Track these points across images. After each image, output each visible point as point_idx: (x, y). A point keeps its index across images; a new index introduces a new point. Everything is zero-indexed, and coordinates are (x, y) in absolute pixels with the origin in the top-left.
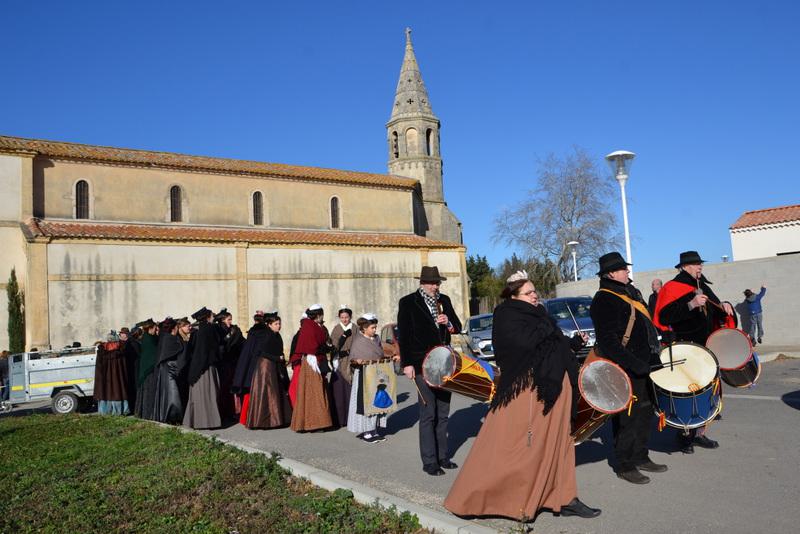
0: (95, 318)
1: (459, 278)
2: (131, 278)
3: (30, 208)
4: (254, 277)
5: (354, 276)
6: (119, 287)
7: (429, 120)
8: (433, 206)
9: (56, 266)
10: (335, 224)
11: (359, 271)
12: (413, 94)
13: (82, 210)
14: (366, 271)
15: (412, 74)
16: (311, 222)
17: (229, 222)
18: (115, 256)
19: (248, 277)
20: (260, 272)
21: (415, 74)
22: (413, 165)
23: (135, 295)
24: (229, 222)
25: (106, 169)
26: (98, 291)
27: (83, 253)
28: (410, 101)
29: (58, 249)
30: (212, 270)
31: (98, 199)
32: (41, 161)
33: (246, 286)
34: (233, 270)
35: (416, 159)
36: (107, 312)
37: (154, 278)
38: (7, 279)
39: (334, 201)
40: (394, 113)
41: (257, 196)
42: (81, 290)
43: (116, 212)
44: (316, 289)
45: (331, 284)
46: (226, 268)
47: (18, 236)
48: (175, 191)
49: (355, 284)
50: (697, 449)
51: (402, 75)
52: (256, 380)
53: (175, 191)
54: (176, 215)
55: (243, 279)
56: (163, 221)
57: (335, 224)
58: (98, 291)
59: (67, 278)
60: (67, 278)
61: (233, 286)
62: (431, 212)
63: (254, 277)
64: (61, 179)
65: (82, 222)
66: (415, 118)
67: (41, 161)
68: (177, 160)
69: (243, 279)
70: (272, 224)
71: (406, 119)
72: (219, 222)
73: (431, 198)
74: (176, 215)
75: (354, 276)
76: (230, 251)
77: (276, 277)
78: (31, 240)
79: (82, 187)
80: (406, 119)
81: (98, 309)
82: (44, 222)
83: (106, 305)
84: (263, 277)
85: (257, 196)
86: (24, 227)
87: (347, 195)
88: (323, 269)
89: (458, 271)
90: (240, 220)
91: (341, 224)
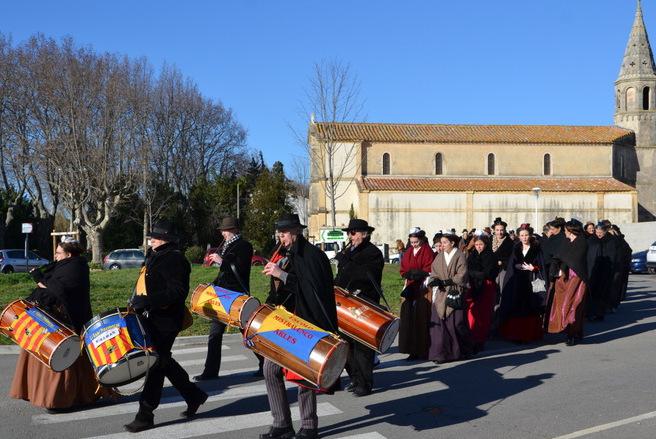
0: (390, 231)
1: (630, 213)
2: (408, 210)
3: (360, 170)
4: (477, 211)
5: (544, 211)
6: (402, 214)
7: (647, 79)
8: (645, 151)
9: (372, 205)
10: (547, 171)
11: (548, 207)
12: (636, 57)
13: (386, 170)
14: (553, 207)
15: (637, 39)
16: (529, 171)
17: (472, 174)
18: (400, 198)
19: (473, 211)
20: (480, 208)
21: (640, 39)
22: (630, 117)
23: (410, 220)
24: (472, 174)
25: (399, 146)
26: (392, 217)
27: (385, 197)
28: (633, 64)
29: (373, 195)
30: (453, 207)
31: (394, 163)
32: (366, 144)
33: (472, 216)
34: (464, 207)
35: (633, 113)
36: (395, 228)
37: (421, 211)
38: (349, 208)
39: (547, 157)
40: (621, 73)
41: (491, 157)
42: (383, 216)
43: (404, 171)
44: (516, 218)
45: (527, 216)
46: (460, 206)
47: (354, 187)
48: (439, 157)
49: (544, 216)
50: (549, 355)
51: (630, 40)
52: (590, 269)
53: (439, 157)
54: (439, 171)
55: (471, 212)
56: (431, 174)
57: (547, 171)
58: (392, 217)
59: (377, 210)
60: (377, 210)
61: (464, 216)
62: (642, 156)
63: (477, 211)
64: (376, 151)
65: (386, 177)
66: (634, 79)
67: (366, 144)
68: (553, 136)
69: (471, 212)
70: (500, 174)
71: (627, 81)
72: (466, 174)
73: (643, 145)
74: (439, 171)
75: (544, 211)
76: (462, 196)
77: (490, 211)
78: (361, 191)
79: (386, 157)
80: (627, 81)
81: (391, 226)
82: (368, 177)
83: (396, 224)
84: (483, 211)
85: (491, 157)
86: (358, 183)
87: (555, 151)
88: (522, 205)
89: (630, 207)
90: (479, 172)
91: (497, 172)
